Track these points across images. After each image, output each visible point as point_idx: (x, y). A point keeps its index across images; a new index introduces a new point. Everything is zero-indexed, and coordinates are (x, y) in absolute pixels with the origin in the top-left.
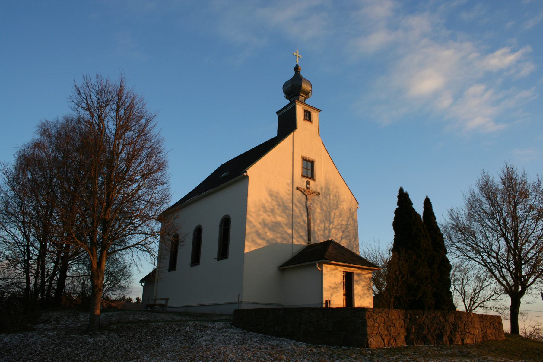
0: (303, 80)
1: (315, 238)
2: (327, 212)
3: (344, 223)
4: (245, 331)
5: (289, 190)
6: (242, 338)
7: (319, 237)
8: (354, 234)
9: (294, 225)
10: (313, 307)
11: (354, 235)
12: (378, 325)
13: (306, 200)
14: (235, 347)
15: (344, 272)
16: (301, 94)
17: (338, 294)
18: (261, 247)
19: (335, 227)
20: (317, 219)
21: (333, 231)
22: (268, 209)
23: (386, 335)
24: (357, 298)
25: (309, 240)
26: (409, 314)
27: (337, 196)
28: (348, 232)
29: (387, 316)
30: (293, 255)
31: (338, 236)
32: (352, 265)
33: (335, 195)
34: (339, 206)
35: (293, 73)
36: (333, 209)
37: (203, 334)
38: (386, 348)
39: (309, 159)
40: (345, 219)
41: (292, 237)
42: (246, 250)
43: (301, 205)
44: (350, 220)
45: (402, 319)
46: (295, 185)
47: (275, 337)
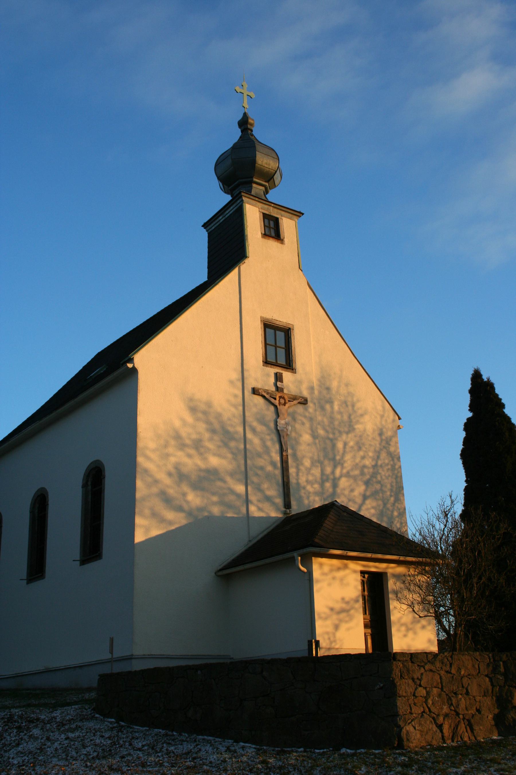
0: (258, 147)
1: (300, 500)
2: (328, 442)
3: (368, 462)
4: (122, 723)
5: (236, 396)
6: (109, 742)
7: (311, 498)
8: (392, 486)
9: (250, 473)
10: (284, 657)
11: (394, 489)
12: (424, 692)
13: (274, 416)
14: (86, 766)
15: (363, 573)
16: (255, 180)
17: (352, 624)
18: (173, 528)
19: (348, 472)
20: (304, 457)
21: (343, 483)
22: (188, 442)
23: (446, 716)
24: (399, 630)
25: (287, 505)
26: (501, 663)
27: (349, 403)
28: (379, 482)
29: (448, 668)
30: (250, 541)
31: (356, 493)
32: (380, 556)
33: (345, 403)
34: (356, 427)
35: (237, 133)
36: (340, 433)
37: (22, 739)
38: (447, 748)
39: (278, 323)
40: (371, 454)
41: (247, 502)
42: (139, 537)
43: (264, 428)
44: (383, 455)
45: (487, 676)
46: (251, 383)
47: (187, 735)
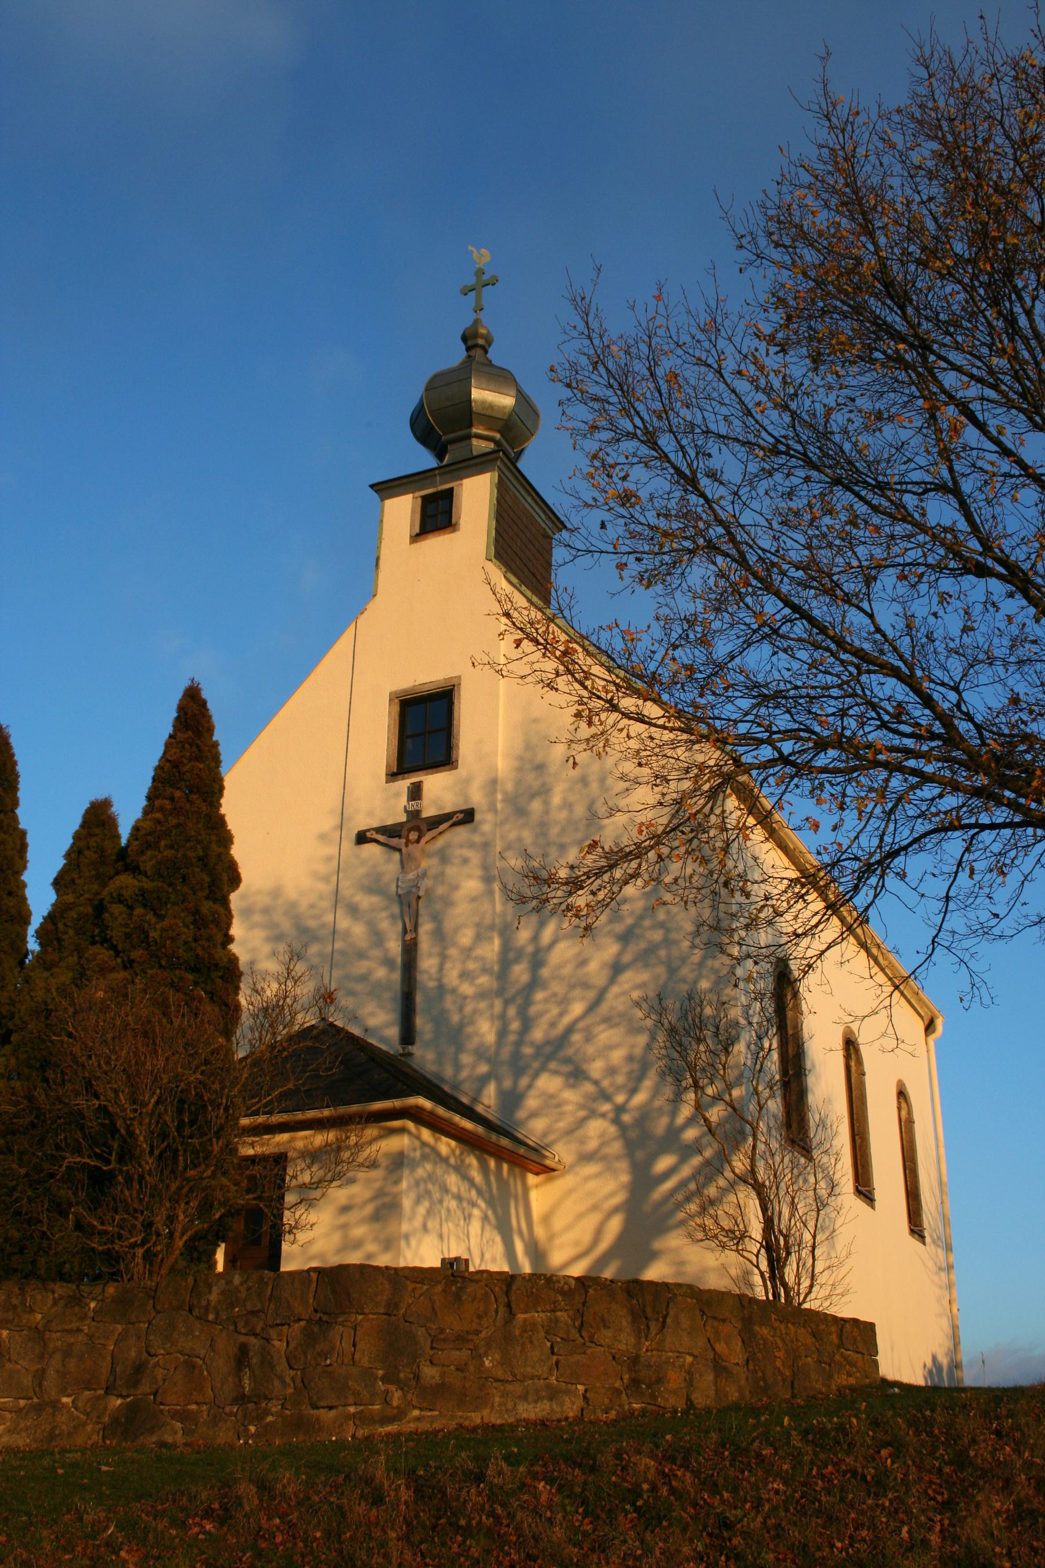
7: (468, 1008)
16: (474, 430)
28: (661, 925)
31: (593, 966)
